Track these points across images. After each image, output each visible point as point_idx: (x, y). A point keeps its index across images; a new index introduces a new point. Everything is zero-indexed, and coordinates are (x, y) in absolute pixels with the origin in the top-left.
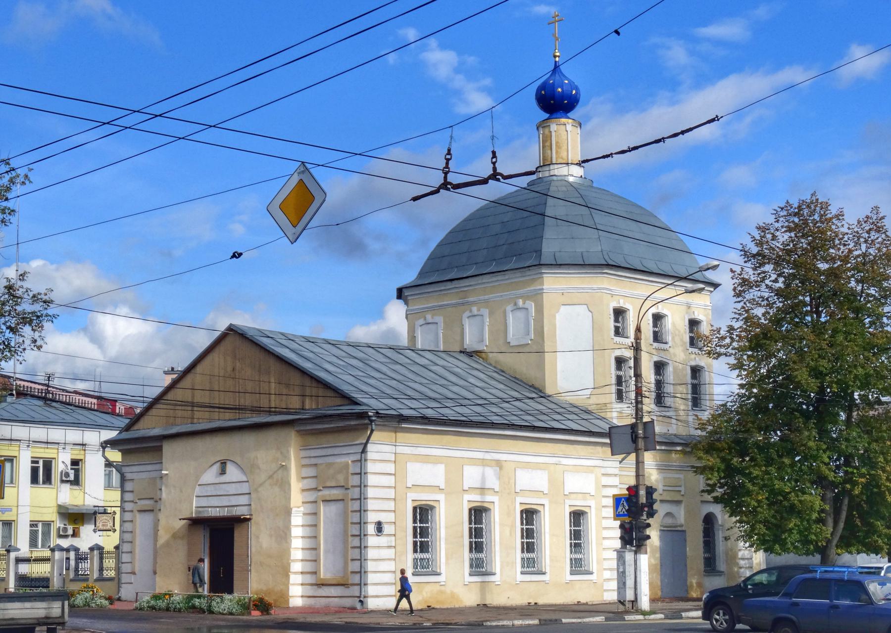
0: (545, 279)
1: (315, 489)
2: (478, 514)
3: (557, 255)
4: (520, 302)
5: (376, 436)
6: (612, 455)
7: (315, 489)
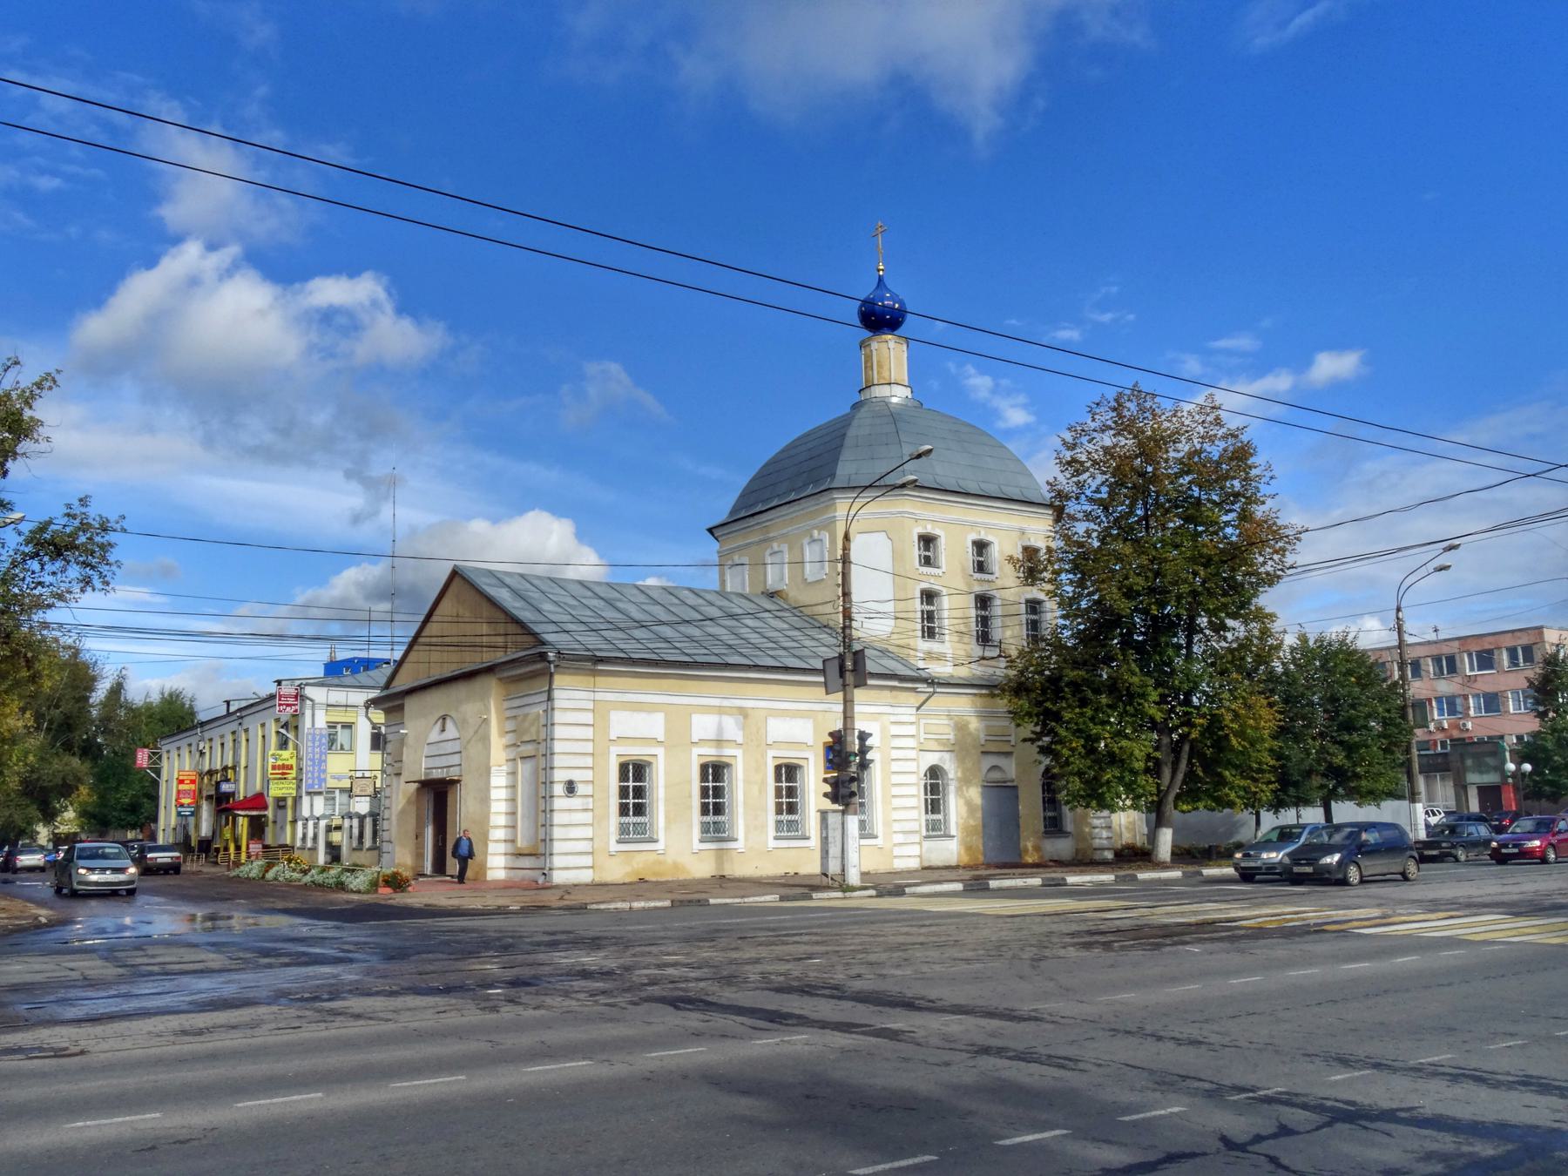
0: (838, 505)
1: (514, 745)
2: (714, 772)
3: (853, 477)
4: (816, 533)
5: (559, 680)
6: (827, 693)
7: (514, 745)
